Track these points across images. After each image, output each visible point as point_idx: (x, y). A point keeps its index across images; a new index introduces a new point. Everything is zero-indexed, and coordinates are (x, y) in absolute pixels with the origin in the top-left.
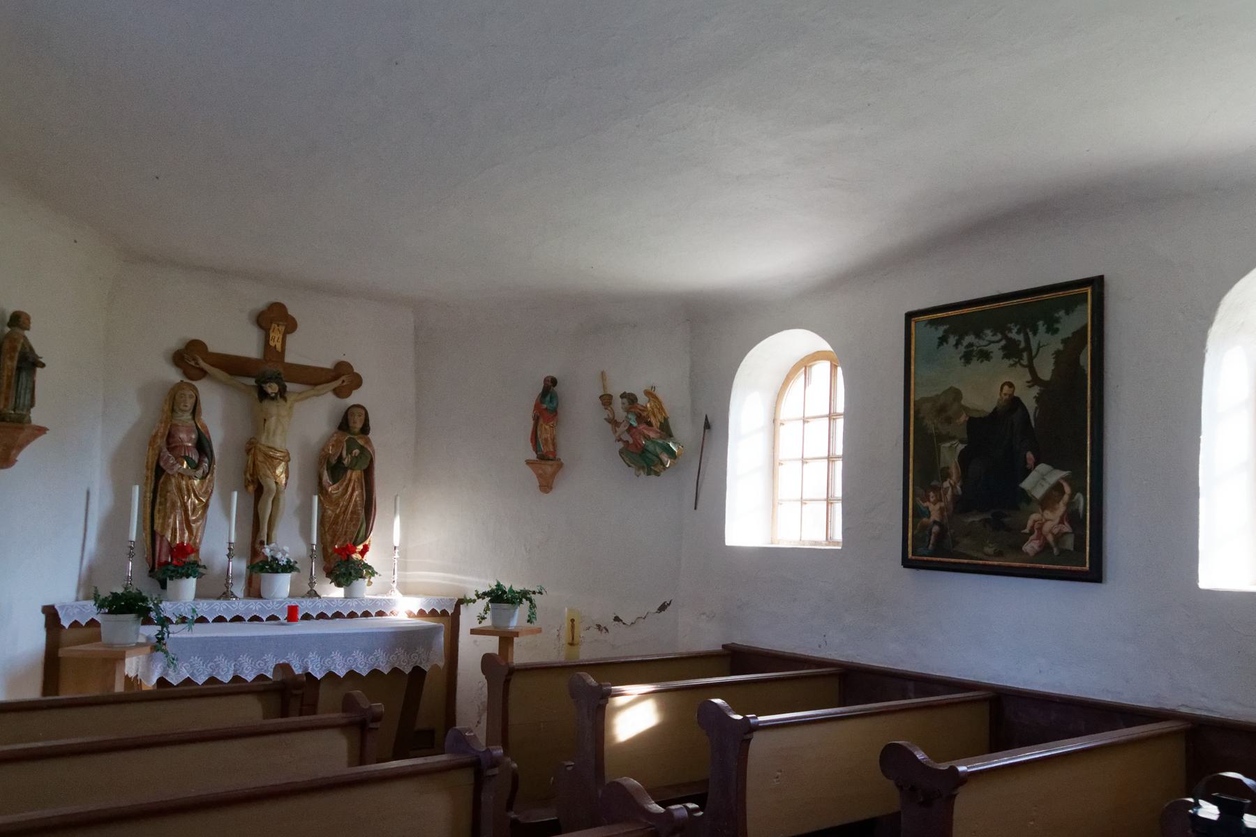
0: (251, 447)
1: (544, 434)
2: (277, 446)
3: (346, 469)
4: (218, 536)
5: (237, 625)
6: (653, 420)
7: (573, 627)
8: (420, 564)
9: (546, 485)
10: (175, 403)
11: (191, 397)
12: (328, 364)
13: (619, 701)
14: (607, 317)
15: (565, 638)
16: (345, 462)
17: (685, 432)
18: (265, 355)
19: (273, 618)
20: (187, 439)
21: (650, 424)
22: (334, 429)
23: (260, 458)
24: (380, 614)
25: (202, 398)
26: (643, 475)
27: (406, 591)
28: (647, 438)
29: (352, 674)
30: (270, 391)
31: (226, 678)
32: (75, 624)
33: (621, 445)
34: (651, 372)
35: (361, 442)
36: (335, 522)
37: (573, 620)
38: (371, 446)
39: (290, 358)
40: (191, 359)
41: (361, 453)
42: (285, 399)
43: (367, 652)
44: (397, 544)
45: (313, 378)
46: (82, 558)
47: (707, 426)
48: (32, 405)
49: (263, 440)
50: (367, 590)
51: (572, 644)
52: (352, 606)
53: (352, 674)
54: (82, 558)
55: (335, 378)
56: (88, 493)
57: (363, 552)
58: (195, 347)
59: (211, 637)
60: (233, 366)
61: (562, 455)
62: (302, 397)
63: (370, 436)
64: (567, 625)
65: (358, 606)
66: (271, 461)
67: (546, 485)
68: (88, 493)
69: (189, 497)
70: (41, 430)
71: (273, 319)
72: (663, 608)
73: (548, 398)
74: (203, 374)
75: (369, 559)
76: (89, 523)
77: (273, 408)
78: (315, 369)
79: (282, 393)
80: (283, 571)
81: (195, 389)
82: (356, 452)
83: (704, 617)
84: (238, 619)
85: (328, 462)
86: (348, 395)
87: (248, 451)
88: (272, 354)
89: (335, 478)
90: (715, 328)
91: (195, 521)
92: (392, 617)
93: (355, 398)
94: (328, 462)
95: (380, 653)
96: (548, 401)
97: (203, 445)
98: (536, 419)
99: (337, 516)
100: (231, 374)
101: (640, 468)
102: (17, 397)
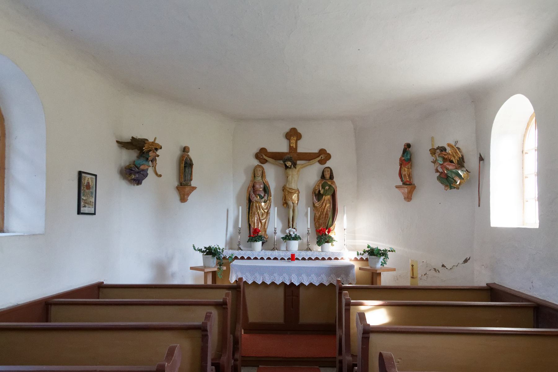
0: (284, 189)
1: (405, 172)
2: (293, 188)
3: (322, 195)
4: (274, 225)
6: (453, 159)
7: (413, 270)
8: (353, 237)
9: (408, 198)
10: (256, 174)
12: (316, 151)
14: (430, 107)
15: (409, 274)
17: (472, 162)
18: (290, 150)
20: (260, 187)
21: (452, 162)
22: (320, 178)
23: (287, 193)
24: (336, 259)
25: (266, 170)
26: (449, 190)
27: (350, 250)
28: (447, 169)
29: (311, 284)
31: (260, 283)
33: (438, 174)
34: (454, 134)
35: (329, 183)
36: (319, 219)
37: (413, 266)
39: (300, 150)
40: (263, 155)
43: (318, 275)
45: (309, 157)
46: (226, 234)
47: (481, 159)
48: (191, 180)
49: (287, 186)
50: (330, 248)
51: (412, 278)
52: (323, 255)
53: (311, 284)
54: (226, 234)
55: (318, 157)
57: (329, 232)
59: (256, 267)
60: (277, 157)
61: (415, 182)
62: (304, 166)
64: (410, 267)
65: (326, 255)
66: (291, 193)
67: (408, 198)
69: (260, 209)
70: (194, 188)
71: (293, 135)
72: (466, 261)
73: (406, 154)
74: (265, 161)
75: (331, 234)
76: (229, 220)
77: (290, 171)
79: (295, 165)
83: (483, 267)
84: (276, 259)
86: (325, 163)
87: (283, 190)
88: (293, 149)
89: (319, 200)
90: (479, 101)
91: (263, 220)
92: (342, 261)
93: (328, 164)
95: (323, 276)
96: (407, 156)
97: (266, 190)
98: (401, 165)
99: (320, 216)
101: (446, 186)
102: (185, 176)
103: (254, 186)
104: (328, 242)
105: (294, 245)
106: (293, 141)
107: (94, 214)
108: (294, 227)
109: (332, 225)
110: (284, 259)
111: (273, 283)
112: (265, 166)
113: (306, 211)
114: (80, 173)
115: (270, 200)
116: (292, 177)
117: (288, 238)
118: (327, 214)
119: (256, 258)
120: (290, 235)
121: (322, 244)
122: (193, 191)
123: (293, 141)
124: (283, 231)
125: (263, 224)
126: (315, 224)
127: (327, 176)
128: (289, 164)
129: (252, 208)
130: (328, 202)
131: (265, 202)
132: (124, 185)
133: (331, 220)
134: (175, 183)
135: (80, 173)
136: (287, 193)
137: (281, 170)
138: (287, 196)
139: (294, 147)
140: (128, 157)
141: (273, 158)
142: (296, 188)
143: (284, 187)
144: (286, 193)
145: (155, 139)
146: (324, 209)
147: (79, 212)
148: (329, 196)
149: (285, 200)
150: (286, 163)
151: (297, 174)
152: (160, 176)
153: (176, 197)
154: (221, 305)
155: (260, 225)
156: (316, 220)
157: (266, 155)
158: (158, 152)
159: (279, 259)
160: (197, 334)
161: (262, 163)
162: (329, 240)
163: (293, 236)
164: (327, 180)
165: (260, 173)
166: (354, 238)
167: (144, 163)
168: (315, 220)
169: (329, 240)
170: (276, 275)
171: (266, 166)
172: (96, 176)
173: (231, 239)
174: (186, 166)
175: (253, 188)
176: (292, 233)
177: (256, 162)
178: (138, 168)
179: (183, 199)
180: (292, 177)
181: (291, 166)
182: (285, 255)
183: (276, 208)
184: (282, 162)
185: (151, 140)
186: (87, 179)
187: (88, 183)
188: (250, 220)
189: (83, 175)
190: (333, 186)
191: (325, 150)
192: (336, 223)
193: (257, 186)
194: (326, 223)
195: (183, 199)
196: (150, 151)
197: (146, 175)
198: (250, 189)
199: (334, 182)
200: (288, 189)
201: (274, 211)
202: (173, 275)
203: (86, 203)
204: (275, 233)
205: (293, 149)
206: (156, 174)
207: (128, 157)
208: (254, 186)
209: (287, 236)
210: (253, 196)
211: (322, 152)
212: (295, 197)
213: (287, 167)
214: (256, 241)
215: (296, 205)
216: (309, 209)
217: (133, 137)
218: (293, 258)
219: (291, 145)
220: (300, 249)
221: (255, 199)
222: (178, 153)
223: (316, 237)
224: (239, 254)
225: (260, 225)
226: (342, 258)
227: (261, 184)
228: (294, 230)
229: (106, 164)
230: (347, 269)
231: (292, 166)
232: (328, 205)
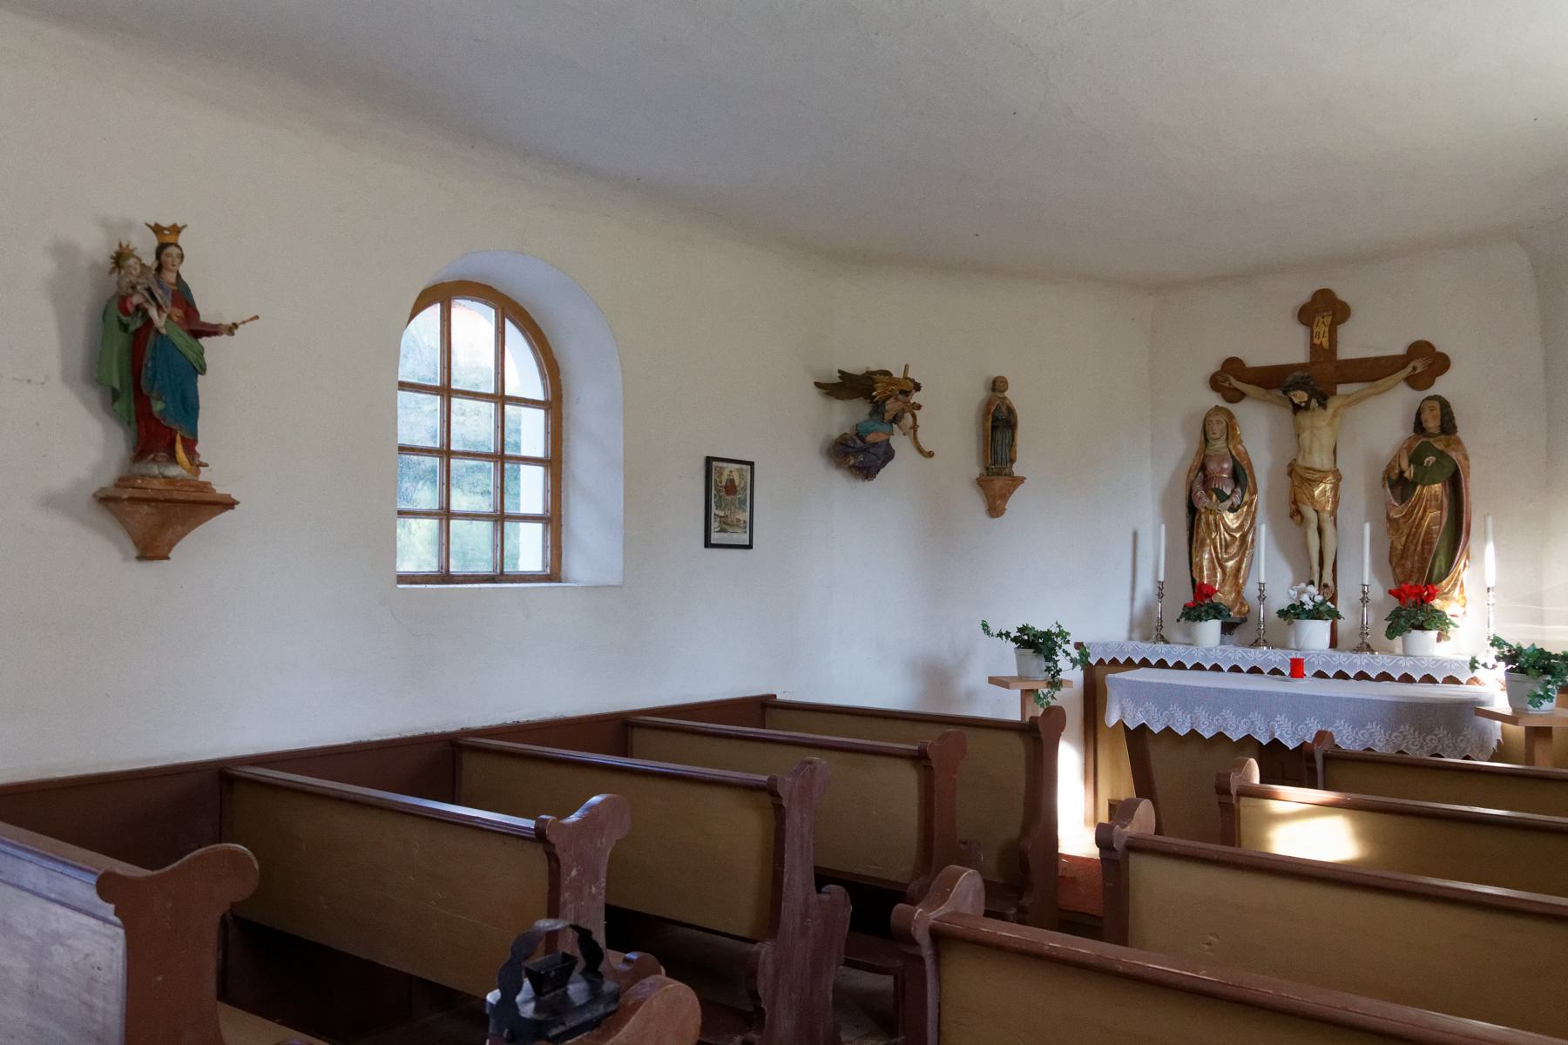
0: (1292, 471)
2: (1317, 466)
4: (1271, 577)
5: (1253, 677)
10: (1214, 433)
11: (1218, 422)
12: (1399, 349)
13: (1275, 806)
16: (1406, 475)
19: (1275, 672)
30: (1296, 401)
31: (1183, 731)
32: (1101, 661)
35: (1439, 446)
36: (1404, 554)
40: (1233, 379)
43: (1358, 724)
44: (1491, 584)
45: (1373, 371)
46: (1133, 599)
48: (1012, 461)
49: (1300, 462)
52: (1406, 666)
54: (1133, 599)
55: (1404, 367)
56: (1135, 535)
58: (1232, 366)
62: (1360, 399)
65: (1415, 667)
68: (1135, 535)
70: (1022, 480)
71: (1324, 310)
77: (1305, 419)
78: (1377, 359)
81: (1230, 416)
84: (1385, 677)
87: (1290, 474)
88: (1323, 354)
89: (1403, 499)
93: (1442, 386)
97: (1240, 475)
100: (1267, 388)
103: (1203, 468)
104: (1421, 627)
105: (1316, 634)
107: (750, 547)
111: (1220, 737)
112: (1238, 410)
114: (709, 461)
118: (1428, 541)
119: (1198, 667)
122: (1015, 487)
127: (1432, 423)
128: (1300, 396)
132: (840, 484)
133: (1441, 562)
134: (973, 468)
135: (709, 461)
137: (1287, 413)
140: (843, 416)
141: (1258, 384)
145: (906, 367)
146: (1419, 526)
147: (708, 544)
149: (1295, 502)
150: (1291, 394)
151: (1330, 424)
152: (930, 455)
153: (975, 503)
154: (919, 758)
155: (1219, 576)
157: (1239, 379)
158: (916, 398)
159: (1266, 671)
160: (766, 799)
161: (1231, 401)
164: (1433, 435)
165: (1218, 429)
166: (1540, 618)
167: (877, 426)
170: (1228, 713)
171: (1240, 410)
172: (751, 464)
173: (1148, 610)
174: (999, 425)
175: (1202, 474)
176: (1305, 598)
177: (1215, 400)
178: (863, 440)
179: (995, 510)
181: (1308, 403)
184: (1280, 393)
185: (898, 373)
186: (726, 473)
187: (732, 481)
189: (715, 464)
190: (1453, 455)
191: (1428, 345)
195: (995, 509)
196: (889, 397)
197: (889, 455)
199: (1459, 442)
200: (1301, 472)
202: (971, 696)
205: (1323, 354)
206: (920, 450)
207: (843, 416)
208: (1203, 468)
209: (1292, 606)
210: (1200, 493)
211: (1420, 349)
212: (1322, 490)
217: (842, 374)
218: (1297, 668)
219: (1317, 341)
221: (1203, 501)
222: (980, 394)
225: (1219, 576)
227: (1223, 460)
229: (785, 438)
231: (1314, 403)
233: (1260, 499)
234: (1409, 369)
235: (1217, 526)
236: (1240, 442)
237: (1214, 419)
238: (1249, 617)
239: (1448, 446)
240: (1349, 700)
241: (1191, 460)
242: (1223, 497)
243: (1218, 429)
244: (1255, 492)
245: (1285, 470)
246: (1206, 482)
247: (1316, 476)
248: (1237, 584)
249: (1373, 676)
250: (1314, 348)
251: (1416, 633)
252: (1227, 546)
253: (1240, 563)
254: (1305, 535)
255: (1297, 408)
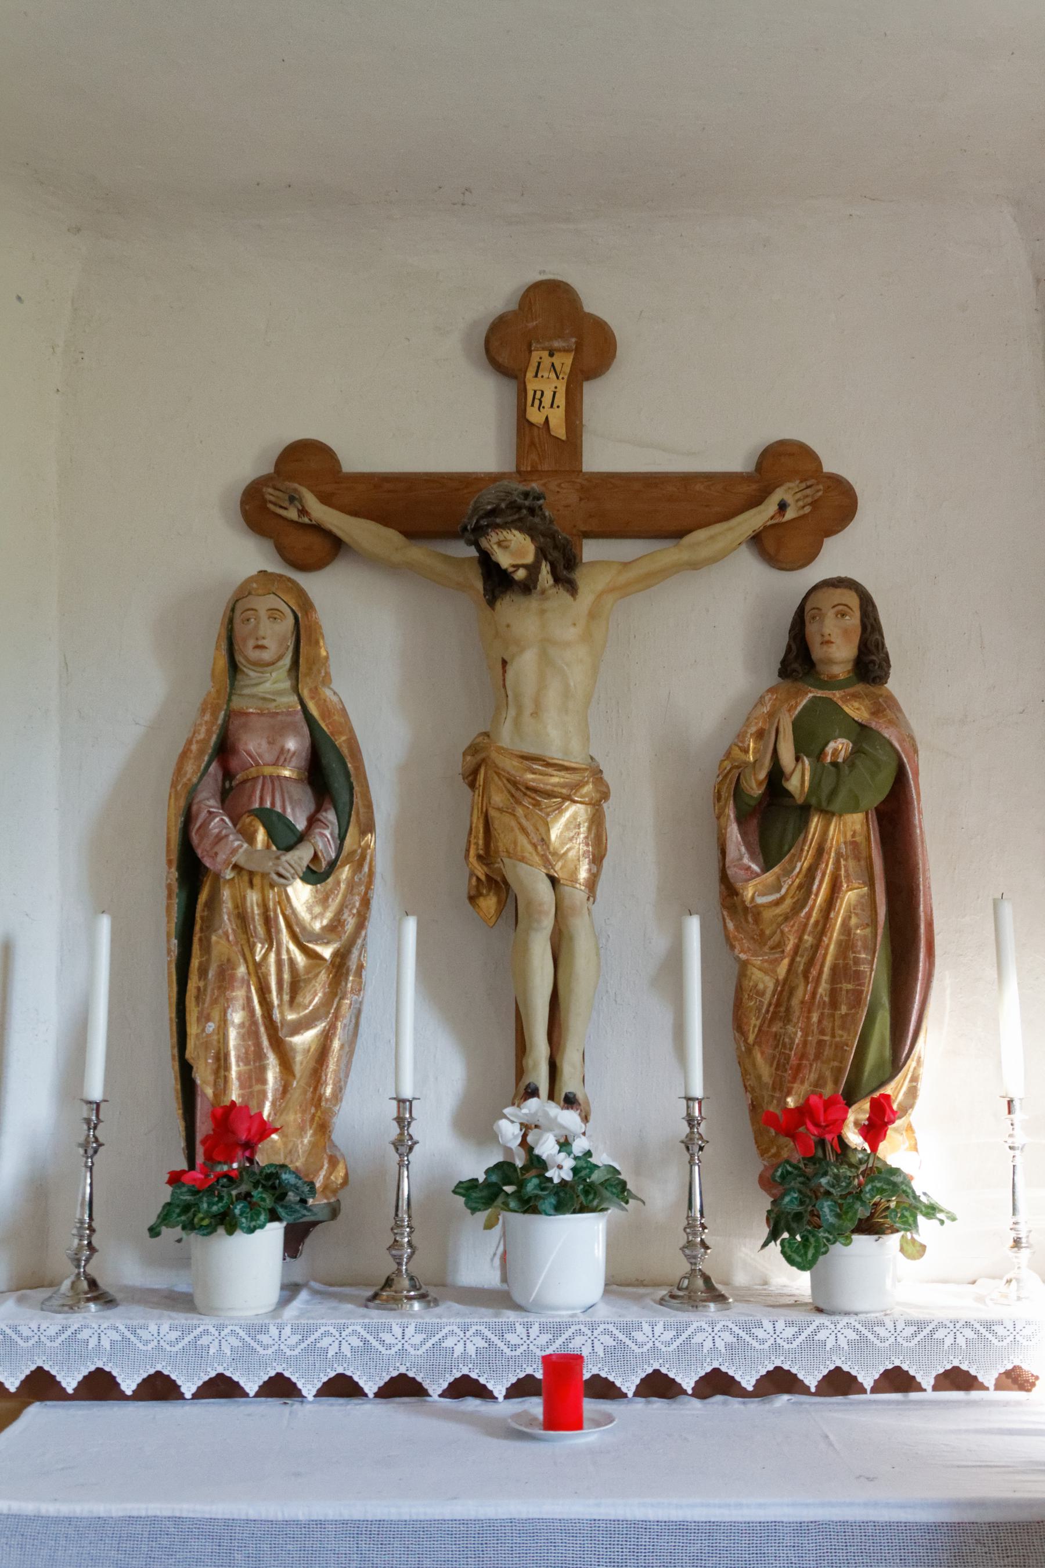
0: (477, 767)
2: (554, 753)
3: (804, 811)
4: (400, 1075)
10: (241, 645)
11: (274, 614)
12: (732, 456)
20: (277, 757)
23: (498, 798)
30: (504, 560)
35: (857, 711)
36: (781, 1008)
38: (897, 719)
40: (302, 505)
41: (857, 751)
42: (572, 587)
44: (698, 1091)
45: (669, 510)
49: (506, 737)
50: (893, 1282)
52: (834, 1345)
55: (756, 501)
57: (875, 1129)
58: (305, 462)
60: (426, 511)
63: (893, 685)
66: (538, 799)
69: (271, 937)
71: (546, 336)
75: (893, 1152)
77: (520, 616)
78: (687, 479)
79: (563, 564)
80: (560, 1208)
82: (839, 747)
85: (738, 792)
87: (471, 778)
88: (546, 449)
89: (770, 852)
94: (738, 792)
97: (329, 774)
99: (785, 989)
100: (411, 534)
104: (871, 1227)
105: (574, 1250)
106: (548, 385)
108: (569, 1084)
109: (896, 1064)
110: (482, 1393)
112: (317, 586)
113: (660, 944)
115: (360, 860)
116: (545, 659)
117: (517, 1188)
120: (537, 1164)
121: (821, 1250)
123: (548, 385)
124: (474, 1123)
125: (301, 1063)
126: (745, 1059)
127: (839, 651)
129: (209, 926)
130: (848, 866)
131: (314, 875)
136: (498, 798)
137: (460, 607)
138: (499, 821)
139: (558, 428)
142: (576, 759)
143: (474, 749)
144: (493, 789)
148: (855, 821)
149: (487, 857)
150: (491, 542)
151: (587, 637)
155: (272, 1075)
156: (754, 1026)
157: (326, 499)
159: (436, 1388)
162: (879, 1206)
163: (561, 1170)
164: (831, 684)
165: (273, 635)
168: (739, 1026)
169: (879, 1206)
171: (330, 591)
176: (547, 1147)
177: (249, 557)
180: (545, 659)
181: (533, 570)
182: (488, 1356)
183: (411, 926)
188: (192, 1029)
190: (889, 733)
192: (935, 1046)
193: (253, 745)
194: (840, 1049)
198: (191, 769)
199: (891, 702)
200: (510, 765)
201: (397, 950)
203: (808, 1179)
204: (404, 1145)
205: (546, 449)
209: (504, 1170)
210: (219, 823)
211: (784, 462)
212: (566, 828)
213: (497, 582)
214: (227, 1222)
215: (578, 894)
216: (694, 926)
218: (563, 1391)
219: (535, 416)
220: (620, 1283)
221: (228, 847)
223: (757, 1166)
224: (73, 1345)
225: (272, 1075)
226: (1016, 1380)
228: (569, 1118)
230: (233, 991)
232: (850, 896)
233: (381, 845)
234: (770, 507)
235: (268, 922)
236: (327, 680)
237: (264, 604)
238: (346, 1200)
239: (877, 711)
240: (801, 1528)
241: (191, 725)
242: (286, 839)
243: (273, 635)
244: (368, 827)
245: (458, 765)
246: (229, 794)
247: (556, 779)
248: (317, 1100)
249: (748, 1383)
250: (527, 434)
251: (861, 1241)
252: (296, 987)
253: (326, 1037)
254: (520, 953)
255: (497, 582)
